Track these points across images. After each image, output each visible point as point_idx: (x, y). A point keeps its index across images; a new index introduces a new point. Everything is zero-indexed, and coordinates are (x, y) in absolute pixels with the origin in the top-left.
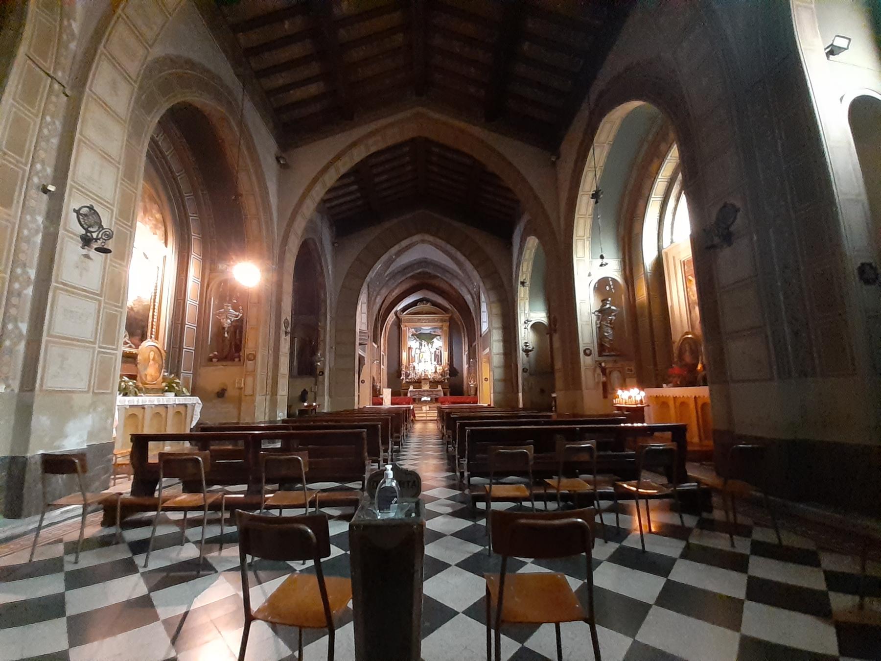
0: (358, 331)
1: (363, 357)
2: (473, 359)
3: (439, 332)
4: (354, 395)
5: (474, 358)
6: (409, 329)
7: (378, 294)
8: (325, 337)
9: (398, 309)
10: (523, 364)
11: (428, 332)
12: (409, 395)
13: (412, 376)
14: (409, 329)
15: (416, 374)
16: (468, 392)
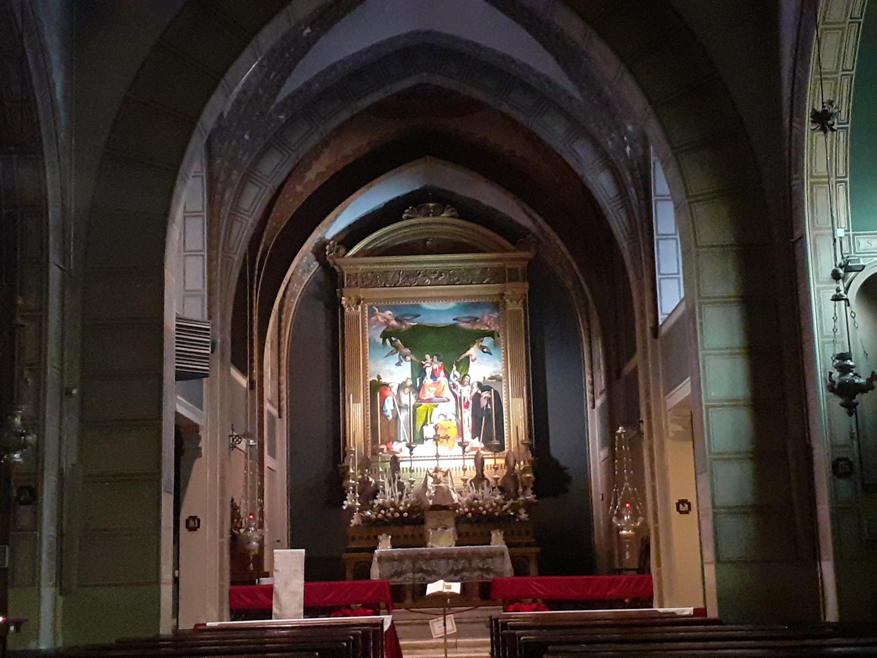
0: (170, 322)
1: (195, 428)
2: (626, 425)
3: (488, 319)
4: (158, 582)
5: (633, 422)
6: (372, 313)
7: (249, 177)
8: (41, 350)
9: (329, 236)
12: (375, 573)
13: (387, 495)
15: (401, 487)
16: (610, 554)
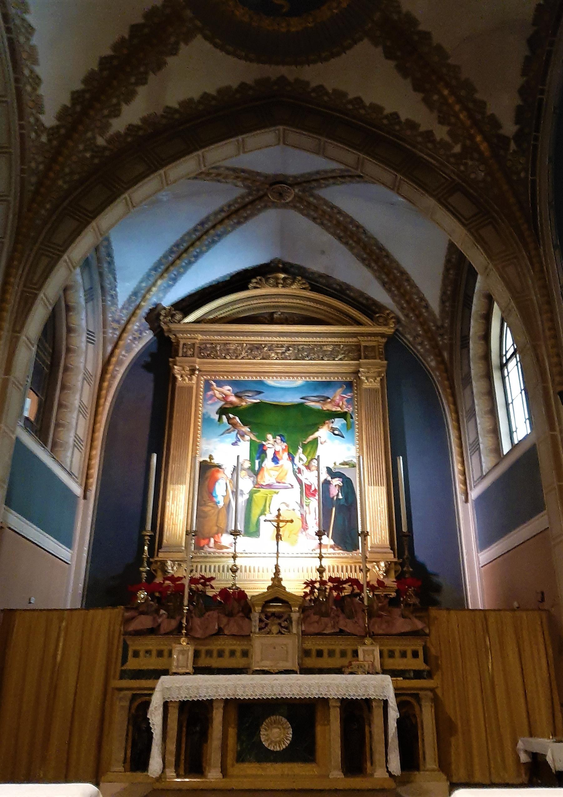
11: (295, 399)
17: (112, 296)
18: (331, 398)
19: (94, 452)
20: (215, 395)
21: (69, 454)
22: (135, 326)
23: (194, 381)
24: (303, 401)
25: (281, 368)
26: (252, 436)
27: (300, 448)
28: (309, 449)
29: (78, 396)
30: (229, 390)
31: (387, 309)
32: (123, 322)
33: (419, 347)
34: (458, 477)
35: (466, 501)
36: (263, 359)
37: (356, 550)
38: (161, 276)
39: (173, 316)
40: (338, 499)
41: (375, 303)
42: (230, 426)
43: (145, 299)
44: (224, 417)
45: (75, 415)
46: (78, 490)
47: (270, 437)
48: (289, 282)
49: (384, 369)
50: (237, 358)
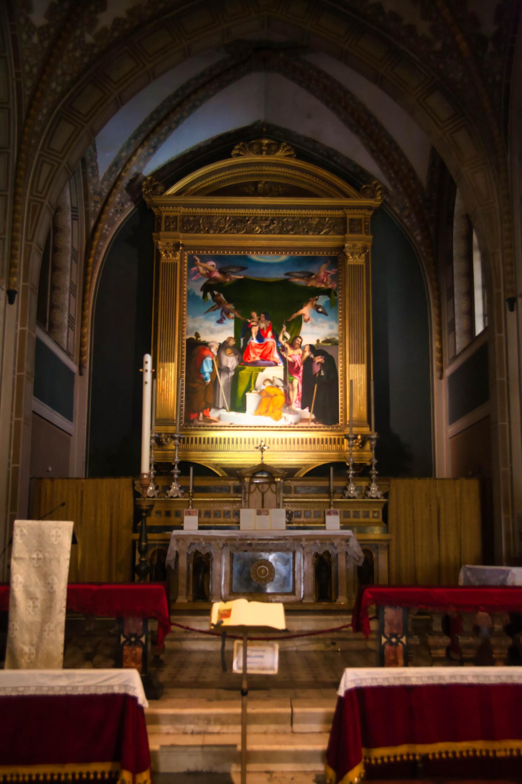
6: (192, 263)
10: (290, 156)
11: (278, 275)
14: (192, 263)
17: (93, 167)
18: (316, 274)
19: (85, 330)
20: (199, 271)
21: (65, 334)
22: (117, 198)
23: (178, 258)
24: (287, 277)
25: (264, 243)
26: (236, 313)
27: (284, 326)
28: (292, 327)
29: (68, 278)
30: (213, 266)
31: (374, 178)
32: (104, 194)
33: (406, 221)
34: (435, 355)
35: (441, 377)
36: (246, 233)
37: (335, 424)
38: (142, 144)
39: (155, 187)
40: (320, 376)
41: (363, 171)
42: (215, 304)
43: (126, 169)
44: (209, 295)
45: (67, 296)
46: (74, 368)
47: (254, 314)
48: (273, 148)
49: (369, 244)
50: (220, 232)
